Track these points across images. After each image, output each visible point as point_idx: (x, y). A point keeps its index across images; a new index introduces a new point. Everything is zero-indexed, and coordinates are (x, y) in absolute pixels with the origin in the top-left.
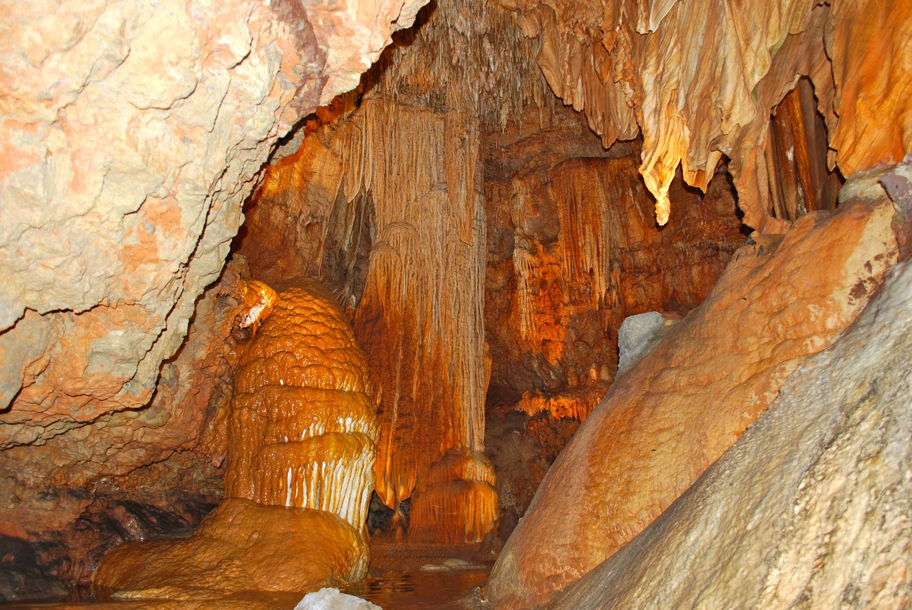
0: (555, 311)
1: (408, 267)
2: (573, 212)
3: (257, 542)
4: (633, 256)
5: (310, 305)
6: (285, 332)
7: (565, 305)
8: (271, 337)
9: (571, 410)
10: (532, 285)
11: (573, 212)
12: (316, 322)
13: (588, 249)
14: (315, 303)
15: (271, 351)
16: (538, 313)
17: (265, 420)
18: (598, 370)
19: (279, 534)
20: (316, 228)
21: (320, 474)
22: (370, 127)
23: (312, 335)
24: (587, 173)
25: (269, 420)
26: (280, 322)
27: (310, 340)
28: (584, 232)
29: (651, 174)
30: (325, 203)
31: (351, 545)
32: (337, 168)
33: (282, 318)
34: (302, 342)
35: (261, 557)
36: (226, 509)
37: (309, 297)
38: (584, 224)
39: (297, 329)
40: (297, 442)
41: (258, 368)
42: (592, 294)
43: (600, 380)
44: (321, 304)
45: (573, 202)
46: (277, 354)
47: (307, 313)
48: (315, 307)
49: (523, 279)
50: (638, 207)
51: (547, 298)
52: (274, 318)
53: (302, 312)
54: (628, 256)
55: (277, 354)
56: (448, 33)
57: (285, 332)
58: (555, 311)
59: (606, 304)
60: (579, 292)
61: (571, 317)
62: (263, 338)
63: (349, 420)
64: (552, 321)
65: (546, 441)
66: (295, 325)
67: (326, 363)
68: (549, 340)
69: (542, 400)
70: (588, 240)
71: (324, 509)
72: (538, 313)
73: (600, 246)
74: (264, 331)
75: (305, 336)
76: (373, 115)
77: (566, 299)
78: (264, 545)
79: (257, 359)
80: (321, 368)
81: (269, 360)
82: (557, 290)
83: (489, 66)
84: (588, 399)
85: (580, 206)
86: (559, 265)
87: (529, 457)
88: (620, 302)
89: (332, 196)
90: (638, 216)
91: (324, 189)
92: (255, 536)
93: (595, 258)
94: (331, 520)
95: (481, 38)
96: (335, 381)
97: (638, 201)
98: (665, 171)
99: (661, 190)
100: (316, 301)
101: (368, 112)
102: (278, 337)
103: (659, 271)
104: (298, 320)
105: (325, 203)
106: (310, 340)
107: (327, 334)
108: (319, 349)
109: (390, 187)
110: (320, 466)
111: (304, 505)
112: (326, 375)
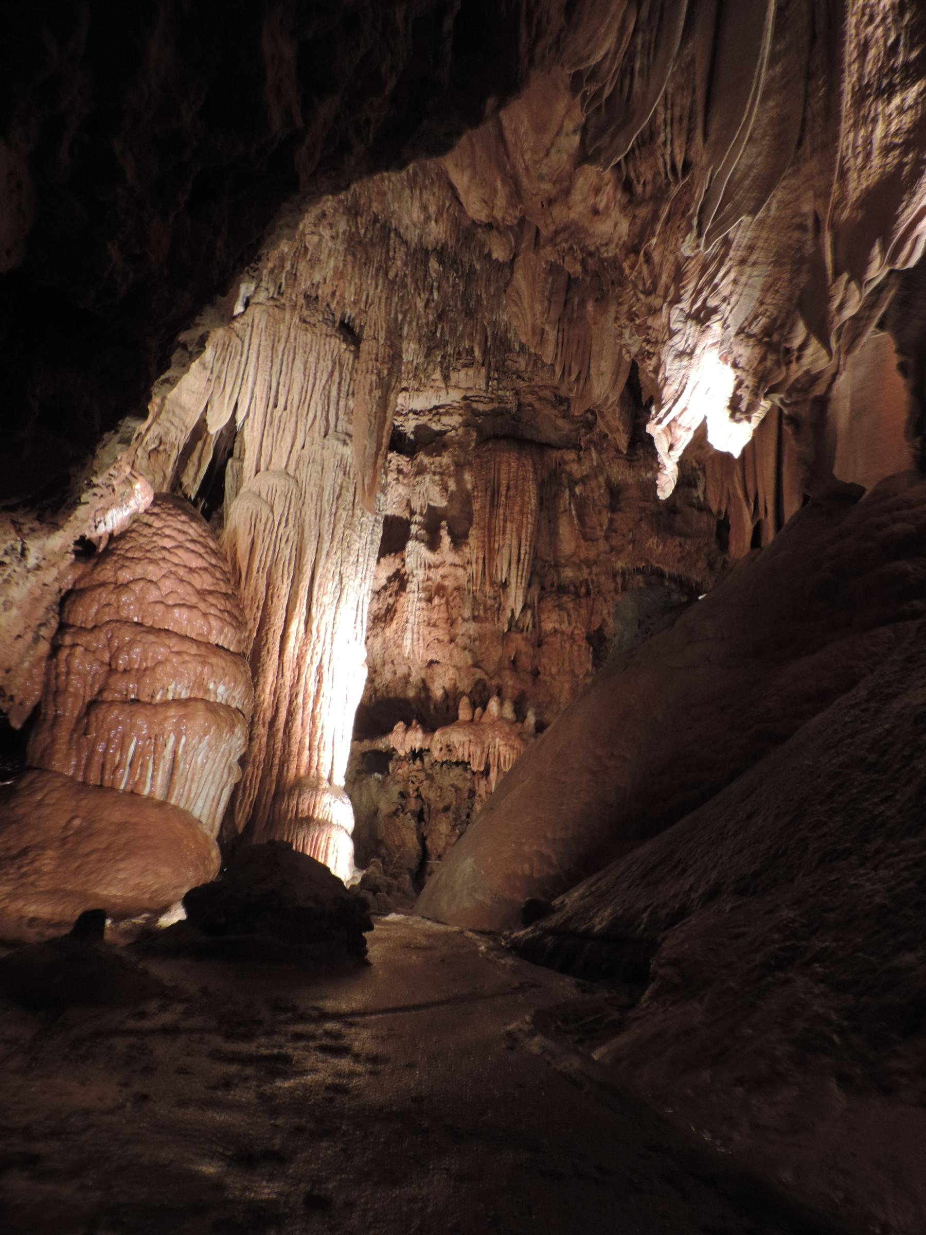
0: (451, 625)
1: (281, 530)
2: (494, 505)
3: (79, 831)
4: (558, 573)
5: (185, 528)
6: (148, 555)
7: (465, 620)
8: (127, 558)
9: (461, 749)
10: (425, 589)
11: (494, 505)
12: (192, 551)
13: (505, 551)
14: (192, 527)
15: (125, 576)
16: (429, 624)
17: (106, 668)
18: (501, 704)
19: (113, 823)
20: (162, 457)
21: (175, 753)
22: (255, 341)
23: (185, 566)
24: (518, 459)
25: (111, 670)
26: (142, 540)
27: (181, 572)
28: (504, 532)
29: (664, 431)
30: (180, 426)
31: (209, 853)
32: (204, 383)
33: (145, 536)
34: (171, 572)
35: (87, 850)
36: (31, 782)
37: (184, 518)
38: (505, 521)
39: (165, 554)
40: (150, 704)
41: (104, 596)
42: (500, 609)
43: (501, 718)
44: (200, 530)
45: (495, 494)
46: (135, 581)
47: (181, 538)
48: (191, 531)
49: (415, 580)
50: (574, 513)
51: (443, 608)
52: (133, 535)
53: (175, 534)
54: (552, 571)
55: (135, 581)
56: (389, 236)
57: (148, 555)
58: (451, 625)
59: (516, 626)
60: (484, 606)
61: (470, 637)
62: (115, 558)
63: (221, 689)
64: (447, 638)
65: (417, 790)
66: (164, 548)
67: (202, 606)
68: (437, 662)
69: (420, 735)
70: (507, 542)
71: (173, 801)
72: (429, 624)
73: (523, 552)
74: (116, 549)
75: (176, 565)
76: (263, 325)
77: (467, 613)
78: (91, 835)
79: (103, 584)
80: (195, 611)
81: (123, 587)
82: (458, 599)
83: (431, 293)
84: (484, 738)
85: (503, 498)
86: (465, 569)
87: (389, 811)
88: (534, 626)
89: (192, 421)
90: (571, 523)
91: (182, 408)
92: (77, 822)
93: (514, 566)
94: (183, 816)
95: (427, 253)
96: (210, 632)
97: (575, 504)
98: (679, 432)
99: (671, 453)
100: (194, 525)
101: (256, 320)
102: (139, 559)
103: (588, 593)
104: (168, 543)
105: (180, 426)
106: (181, 572)
107: (205, 569)
108: (193, 586)
109: (271, 423)
110: (178, 741)
111: (146, 792)
112: (200, 621)
